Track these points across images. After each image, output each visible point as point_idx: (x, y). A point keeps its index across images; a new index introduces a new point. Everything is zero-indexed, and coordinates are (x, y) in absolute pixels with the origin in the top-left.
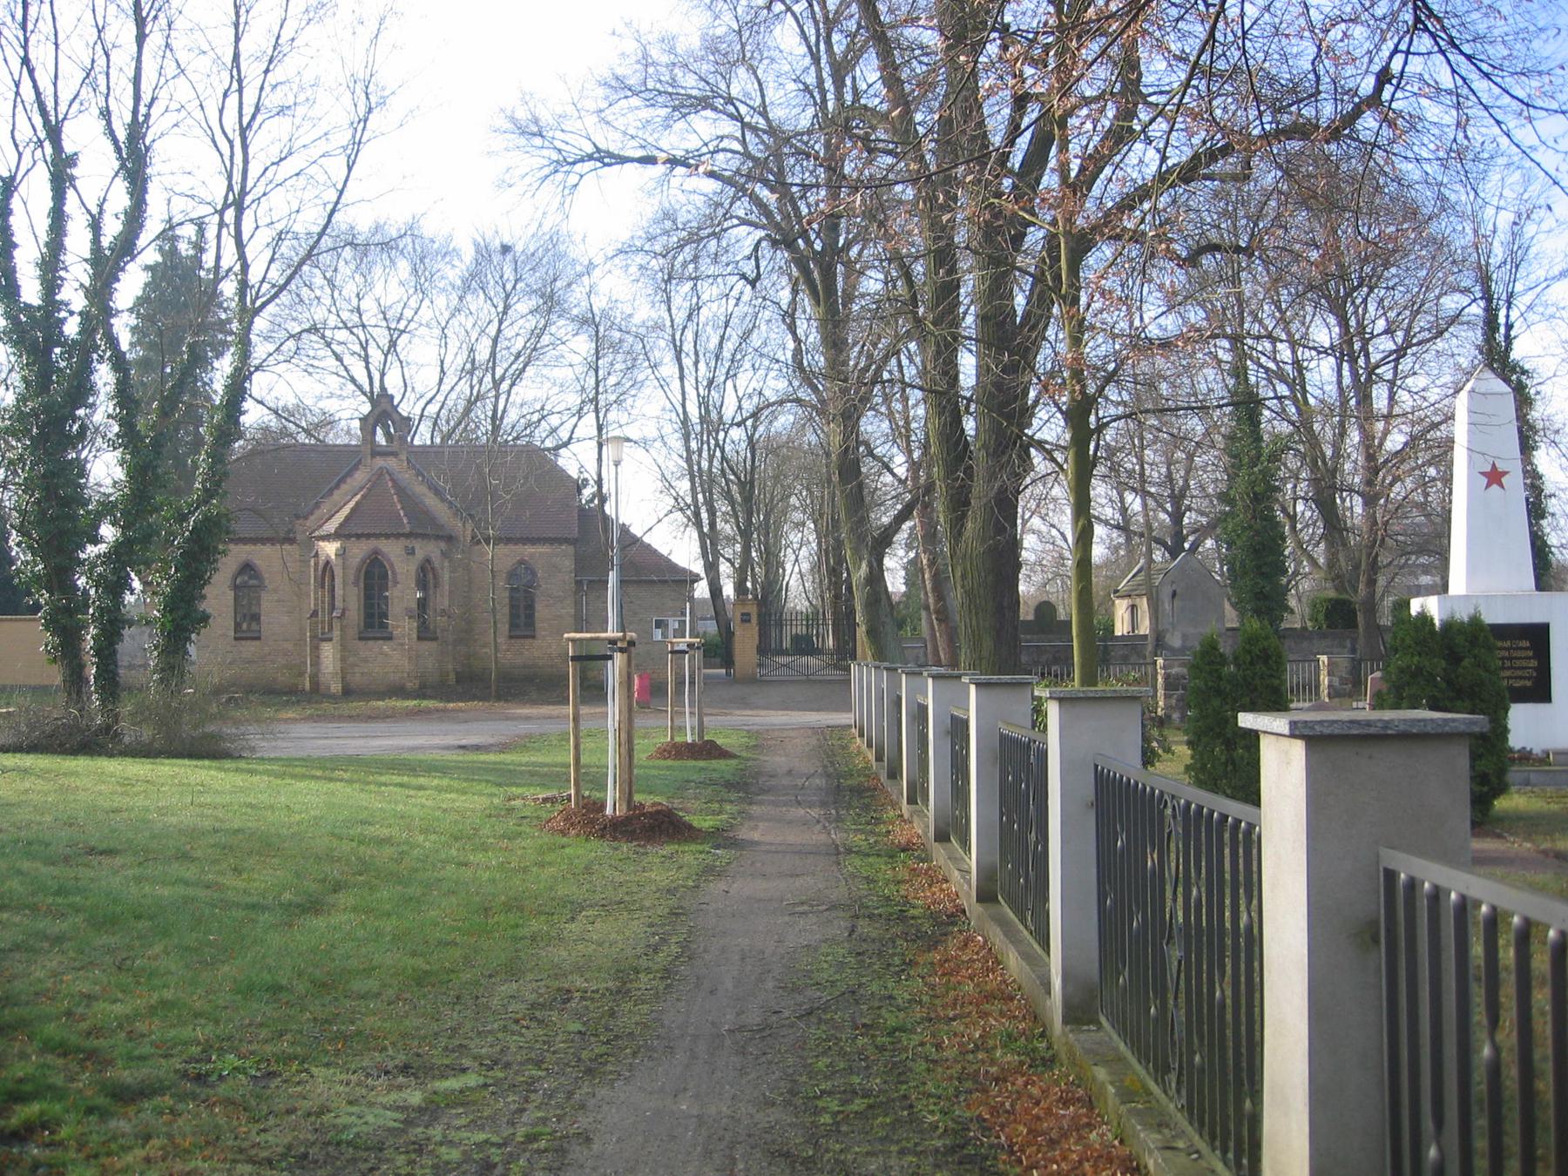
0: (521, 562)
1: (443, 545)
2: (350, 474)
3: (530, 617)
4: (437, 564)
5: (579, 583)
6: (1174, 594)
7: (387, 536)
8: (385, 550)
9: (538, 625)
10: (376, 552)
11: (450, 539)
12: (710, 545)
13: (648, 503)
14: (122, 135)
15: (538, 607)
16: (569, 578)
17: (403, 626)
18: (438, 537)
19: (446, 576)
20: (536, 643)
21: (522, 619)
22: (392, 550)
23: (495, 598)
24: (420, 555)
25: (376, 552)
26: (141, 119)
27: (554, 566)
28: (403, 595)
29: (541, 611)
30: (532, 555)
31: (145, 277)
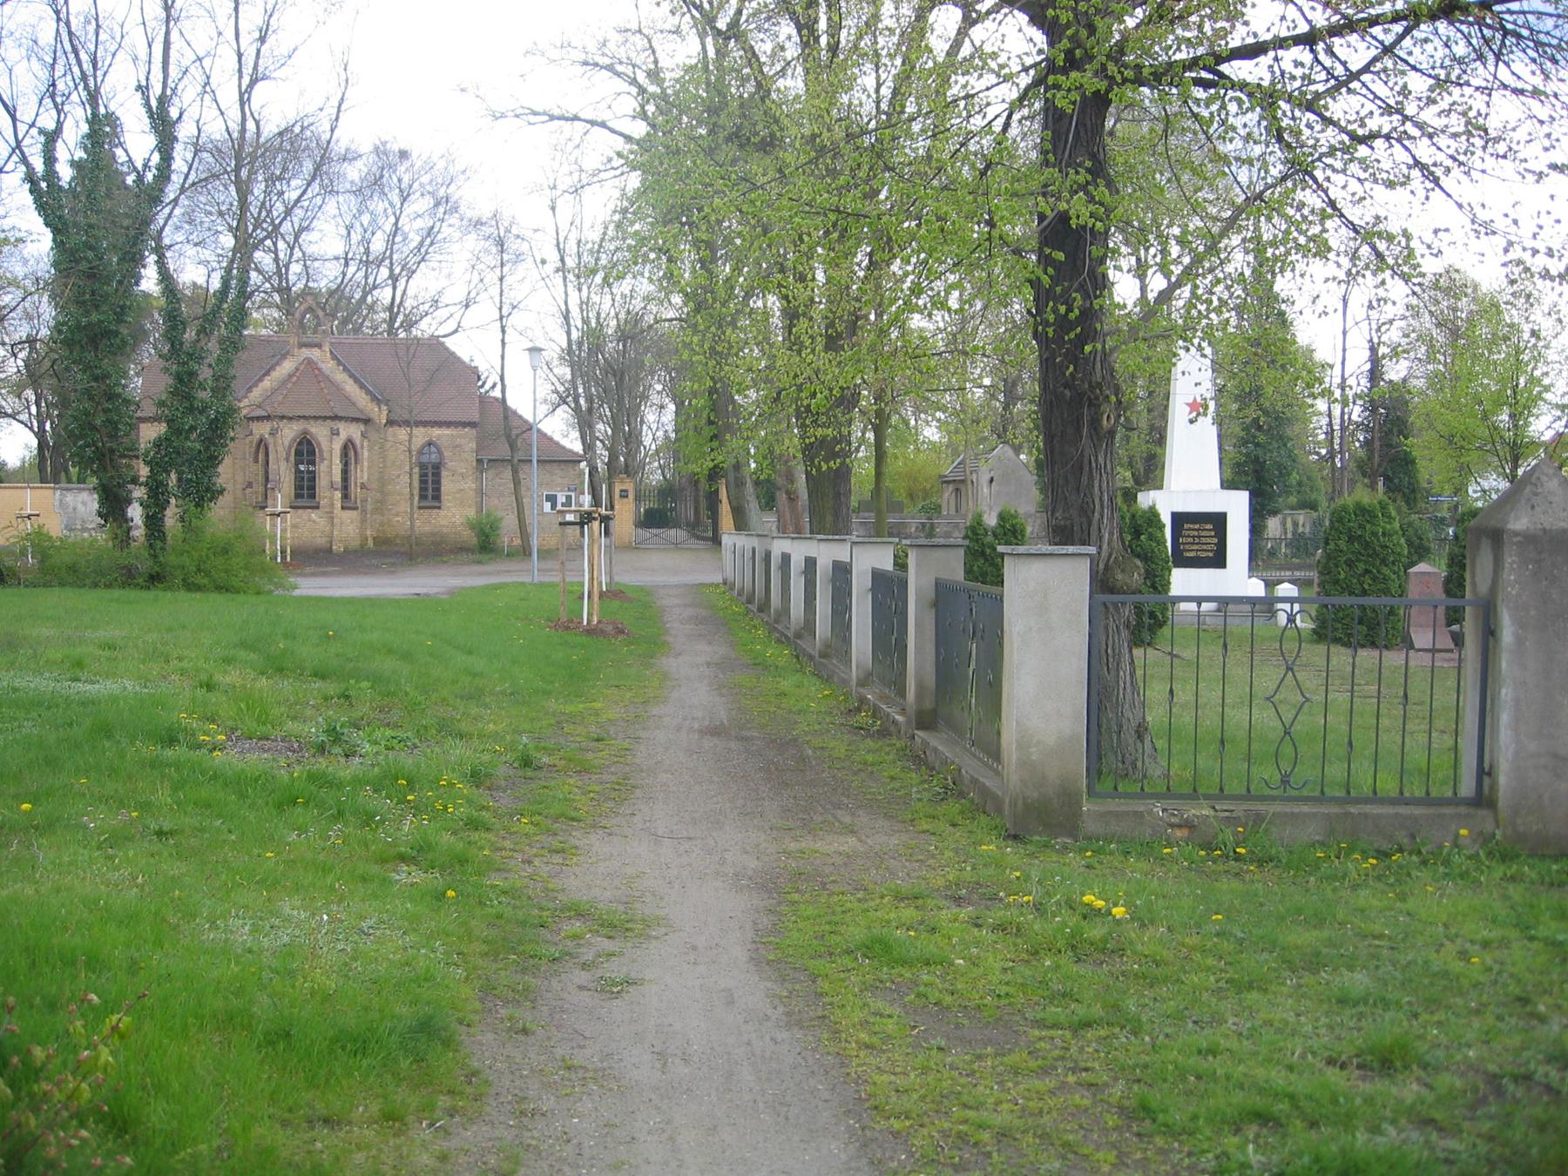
0: (430, 444)
1: (362, 427)
2: (261, 380)
3: (437, 490)
4: (358, 442)
5: (479, 461)
6: (992, 480)
7: (315, 418)
8: (313, 430)
9: (444, 497)
10: (305, 432)
11: (367, 421)
12: (584, 422)
13: (533, 393)
14: (154, 103)
15: (444, 482)
16: (472, 458)
17: (329, 495)
18: (356, 420)
19: (366, 454)
20: (442, 513)
21: (430, 488)
22: (319, 432)
23: (404, 483)
24: (343, 436)
25: (305, 432)
26: (169, 92)
27: (458, 449)
28: (329, 470)
29: (447, 485)
30: (439, 437)
31: (1207, 431)
